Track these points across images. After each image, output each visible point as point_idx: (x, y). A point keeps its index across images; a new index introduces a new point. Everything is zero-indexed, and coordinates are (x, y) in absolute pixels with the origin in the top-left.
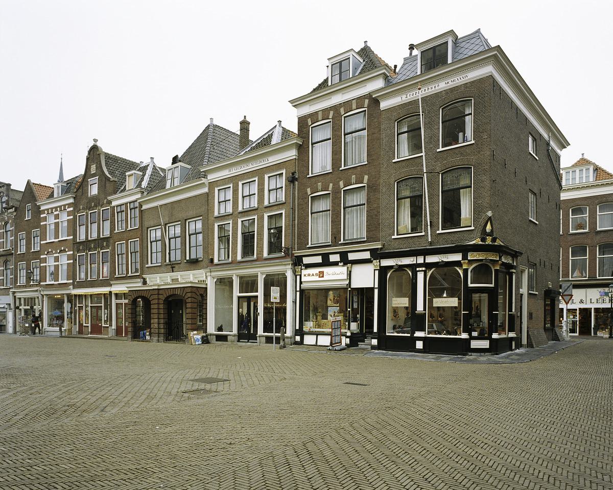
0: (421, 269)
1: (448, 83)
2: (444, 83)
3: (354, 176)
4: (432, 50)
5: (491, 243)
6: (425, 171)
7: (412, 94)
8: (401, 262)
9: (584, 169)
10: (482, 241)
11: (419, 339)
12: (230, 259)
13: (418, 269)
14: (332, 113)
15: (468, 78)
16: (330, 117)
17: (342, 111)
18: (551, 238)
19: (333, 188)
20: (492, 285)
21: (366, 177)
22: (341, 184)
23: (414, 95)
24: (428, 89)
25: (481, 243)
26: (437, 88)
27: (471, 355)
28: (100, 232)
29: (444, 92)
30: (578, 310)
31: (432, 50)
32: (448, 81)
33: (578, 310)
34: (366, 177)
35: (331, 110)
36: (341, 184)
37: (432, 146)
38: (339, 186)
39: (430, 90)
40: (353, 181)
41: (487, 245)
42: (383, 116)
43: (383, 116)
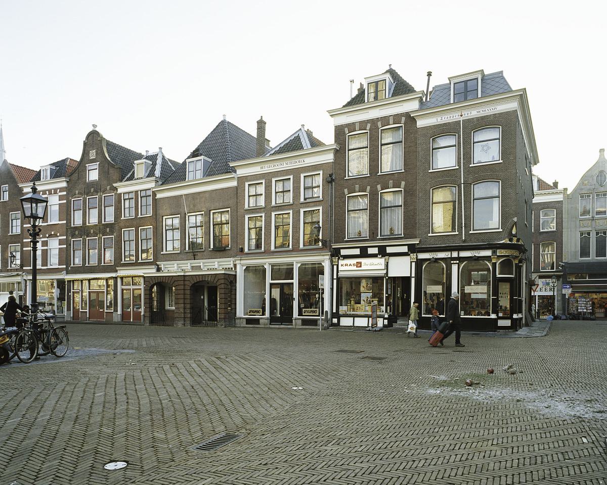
1: (479, 112)
10: (510, 241)
19: (370, 190)
29: (475, 119)
36: (379, 187)
40: (357, 189)
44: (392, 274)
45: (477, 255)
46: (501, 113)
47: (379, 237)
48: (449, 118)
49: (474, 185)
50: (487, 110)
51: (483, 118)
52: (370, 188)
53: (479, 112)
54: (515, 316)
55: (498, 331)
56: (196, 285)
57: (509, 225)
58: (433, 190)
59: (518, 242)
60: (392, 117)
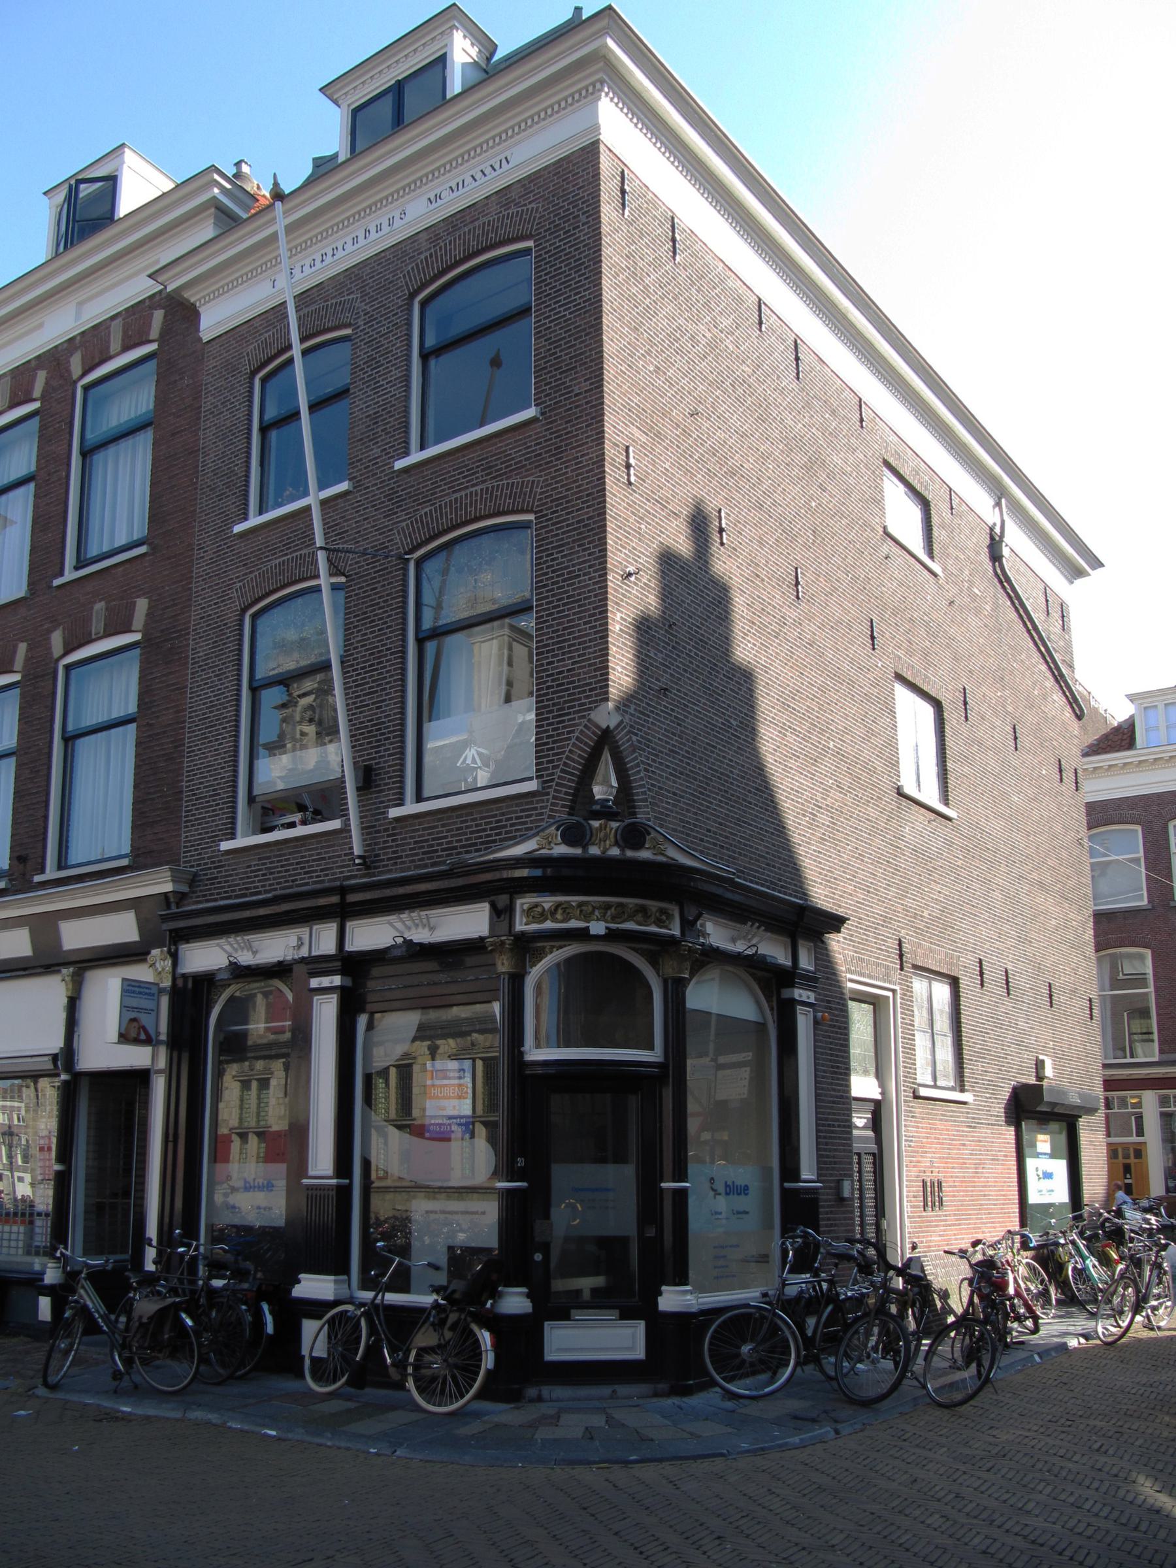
0: (326, 981)
1: (438, 197)
2: (424, 200)
3: (100, 606)
4: (389, 97)
5: (615, 852)
6: (319, 542)
7: (308, 262)
8: (255, 953)
9: (1161, 707)
10: (568, 840)
11: (315, 1308)
12: (897, 987)
13: (315, 983)
14: (42, 376)
15: (511, 165)
16: (37, 393)
17: (76, 364)
18: (1041, 885)
19: (28, 659)
20: (653, 1056)
21: (142, 605)
22: (57, 640)
23: (318, 265)
24: (367, 231)
25: (561, 850)
26: (398, 223)
27: (540, 1399)
28: (217, 924)
29: (424, 236)
30: (1140, 1139)
31: (389, 97)
32: (438, 191)
33: (1140, 1139)
34: (142, 605)
35: (38, 367)
36: (57, 640)
37: (376, 451)
38: (49, 648)
39: (373, 236)
40: (97, 626)
41: (595, 860)
42: (212, 363)
43: (212, 363)
44: (149, 1049)
45: (421, 936)
46: (533, 178)
47: (51, 873)
48: (386, 229)
49: (254, 617)
50: (468, 180)
51: (453, 222)
52: (29, 649)
53: (438, 197)
54: (672, 1299)
55: (532, 1392)
56: (668, 1094)
57: (574, 753)
58: (419, 563)
59: (639, 846)
60: (119, 321)
